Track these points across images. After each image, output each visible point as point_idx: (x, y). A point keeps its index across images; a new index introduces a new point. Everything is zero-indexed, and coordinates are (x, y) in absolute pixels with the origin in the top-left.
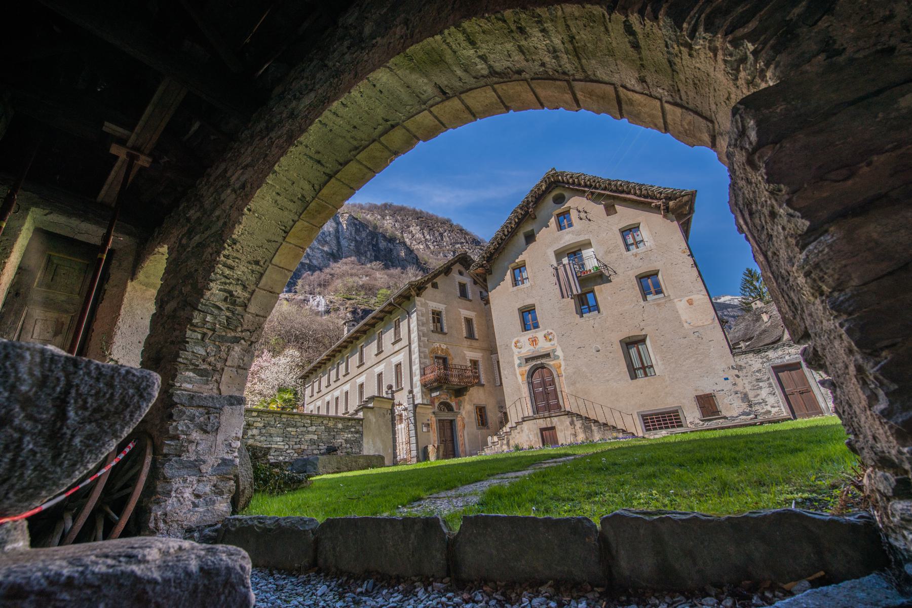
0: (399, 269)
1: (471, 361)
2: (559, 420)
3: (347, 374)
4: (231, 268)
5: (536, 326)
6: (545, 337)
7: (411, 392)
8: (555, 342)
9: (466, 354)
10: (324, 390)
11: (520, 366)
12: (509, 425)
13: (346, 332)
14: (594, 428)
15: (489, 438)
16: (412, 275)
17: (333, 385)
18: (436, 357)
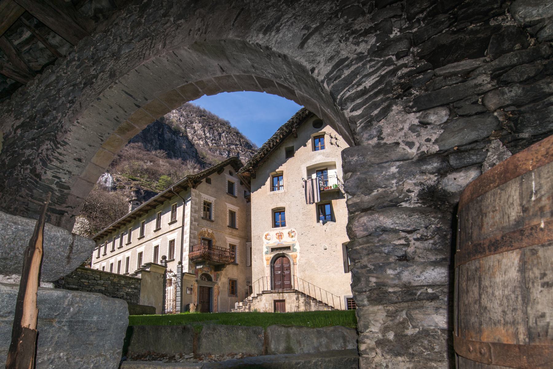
0: (180, 159)
1: (230, 245)
2: (289, 296)
3: (129, 243)
4: (61, 162)
5: (284, 225)
6: (289, 233)
7: (180, 263)
8: (295, 238)
9: (228, 239)
10: (109, 254)
11: (266, 253)
12: (252, 295)
13: (130, 209)
14: (312, 304)
15: (236, 304)
16: (191, 169)
17: (117, 251)
18: (203, 239)
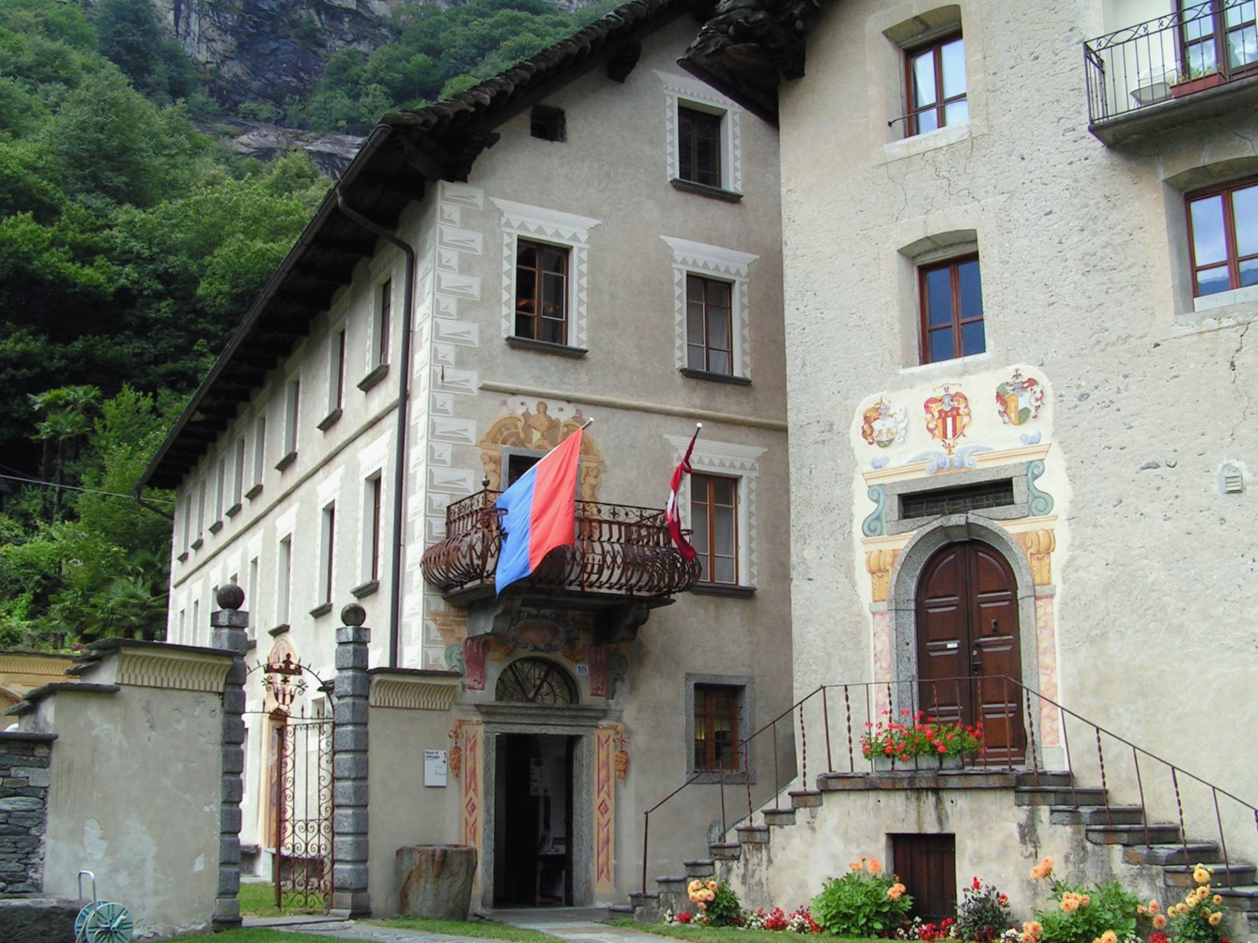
6: (1000, 397)
8: (1042, 427)
11: (872, 528)
12: (796, 785)
